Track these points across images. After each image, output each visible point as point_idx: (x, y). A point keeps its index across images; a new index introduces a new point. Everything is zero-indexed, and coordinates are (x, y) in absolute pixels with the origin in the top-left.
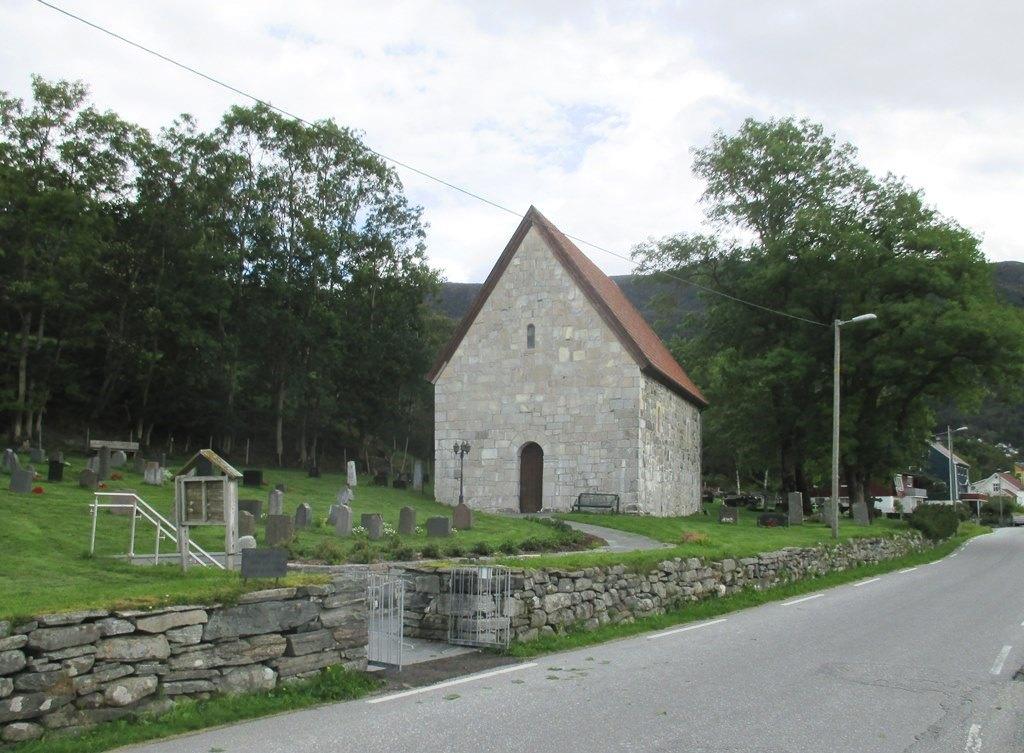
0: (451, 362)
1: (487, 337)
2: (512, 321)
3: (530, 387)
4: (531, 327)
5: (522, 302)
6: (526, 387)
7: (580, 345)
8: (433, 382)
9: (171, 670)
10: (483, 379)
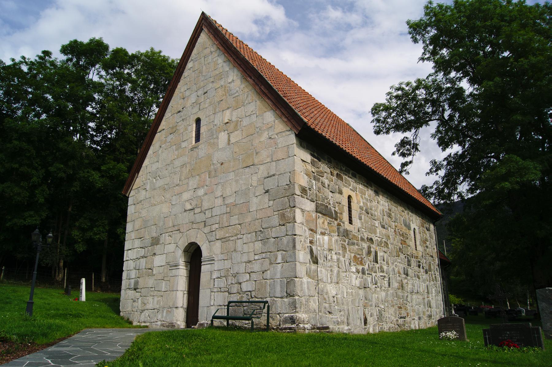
3: (193, 183)
7: (237, 125)
8: (127, 195)
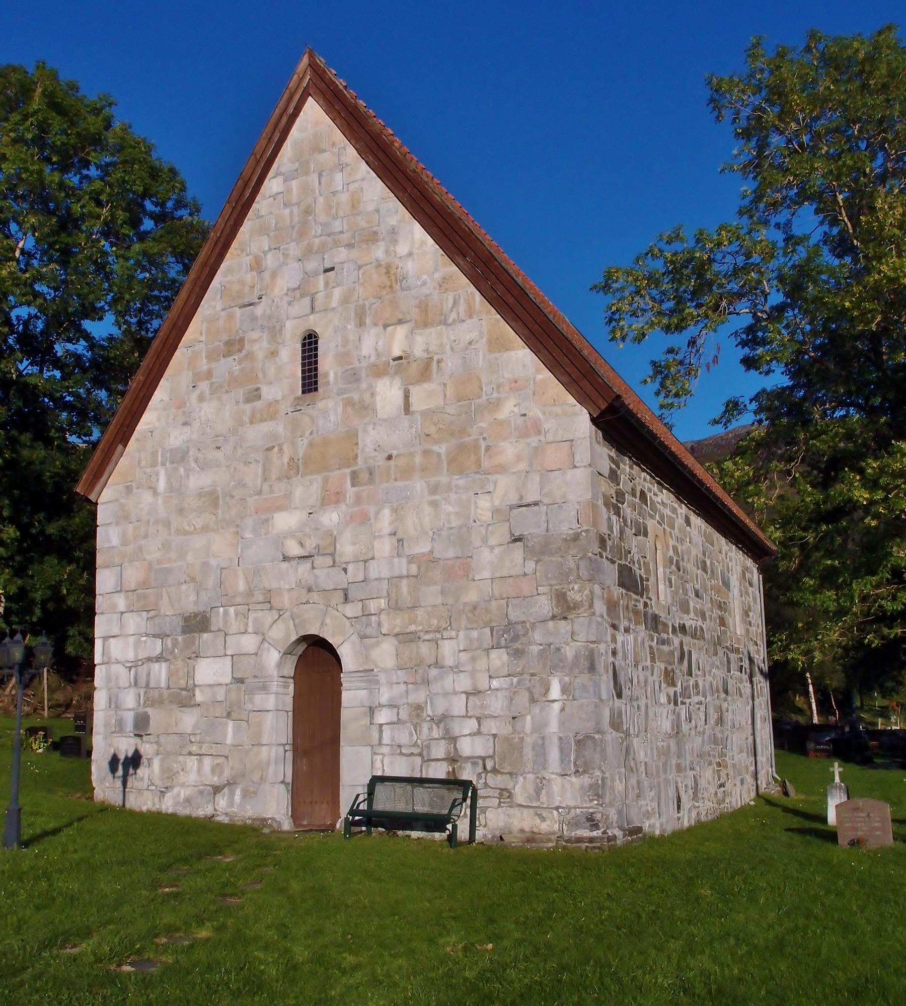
1: (209, 374)
4: (310, 343)
5: (288, 279)
8: (92, 497)
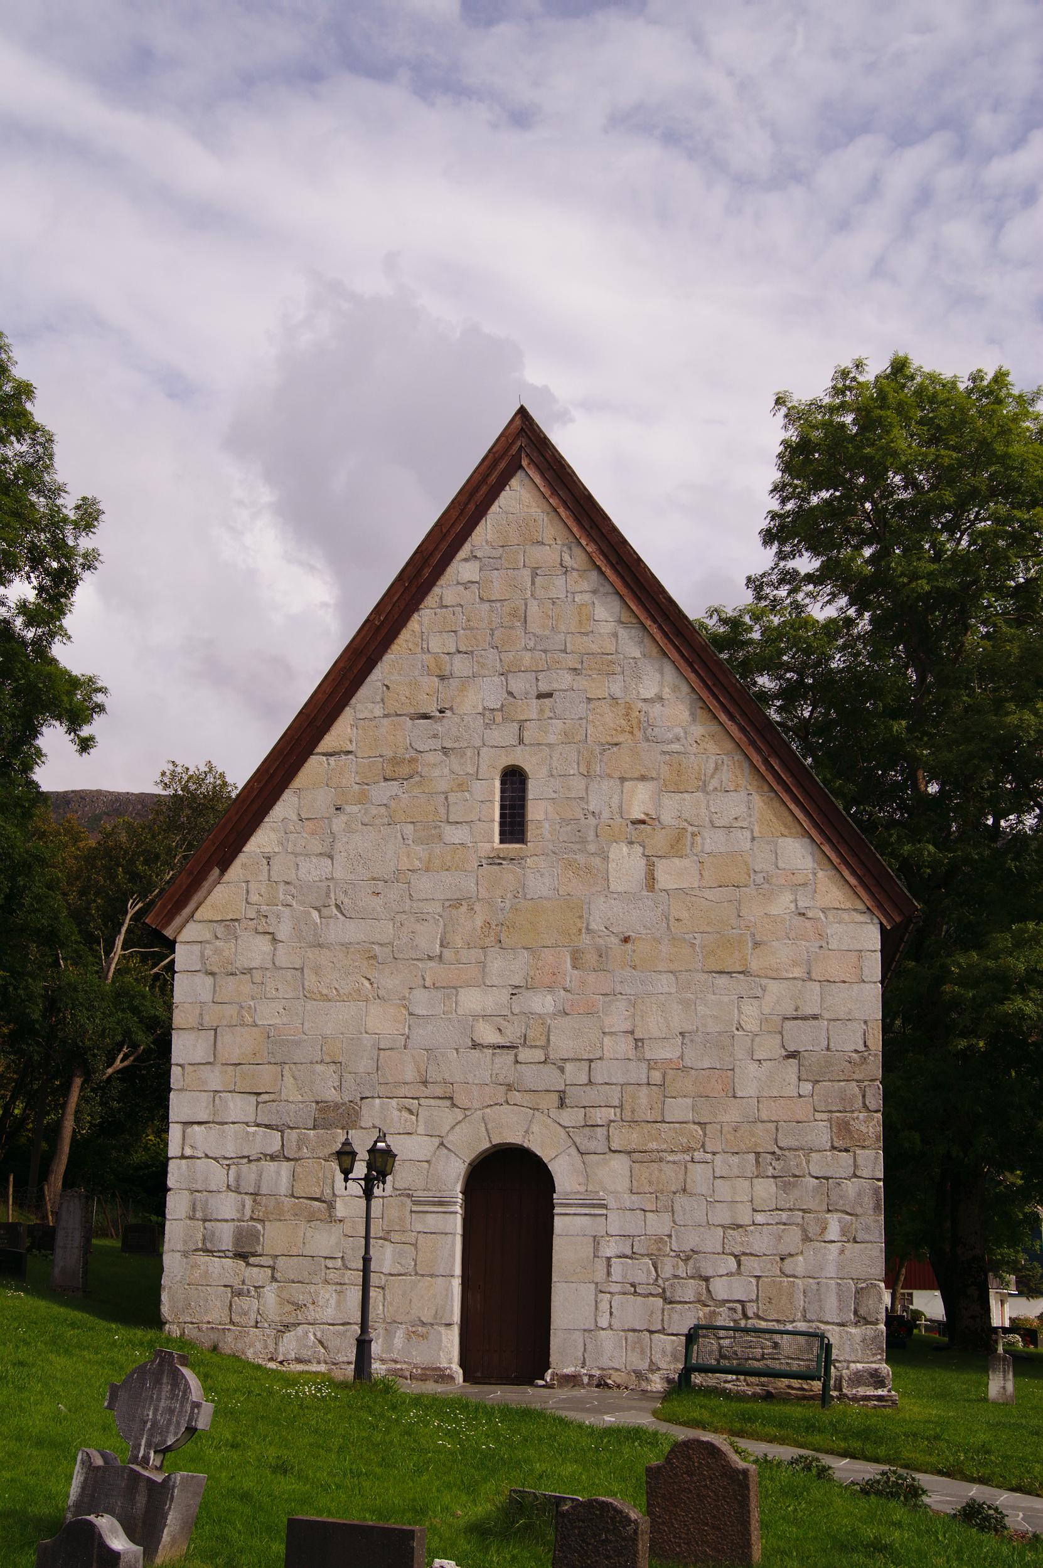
0: (236, 870)
1: (363, 799)
2: (445, 751)
6: (497, 964)
9: (451, 1098)
10: (340, 930)
